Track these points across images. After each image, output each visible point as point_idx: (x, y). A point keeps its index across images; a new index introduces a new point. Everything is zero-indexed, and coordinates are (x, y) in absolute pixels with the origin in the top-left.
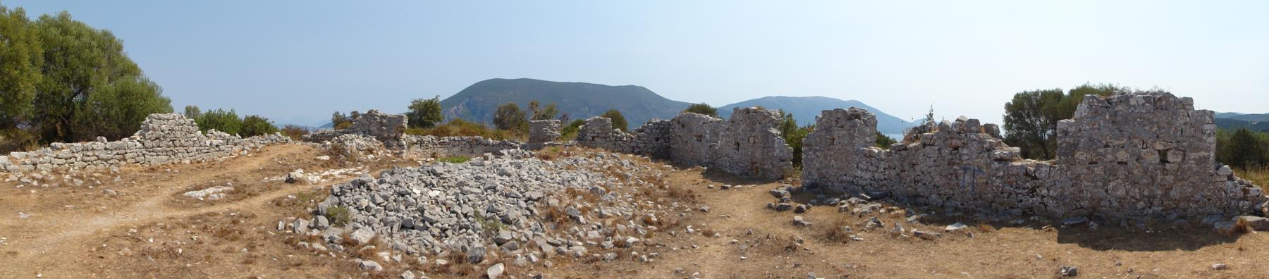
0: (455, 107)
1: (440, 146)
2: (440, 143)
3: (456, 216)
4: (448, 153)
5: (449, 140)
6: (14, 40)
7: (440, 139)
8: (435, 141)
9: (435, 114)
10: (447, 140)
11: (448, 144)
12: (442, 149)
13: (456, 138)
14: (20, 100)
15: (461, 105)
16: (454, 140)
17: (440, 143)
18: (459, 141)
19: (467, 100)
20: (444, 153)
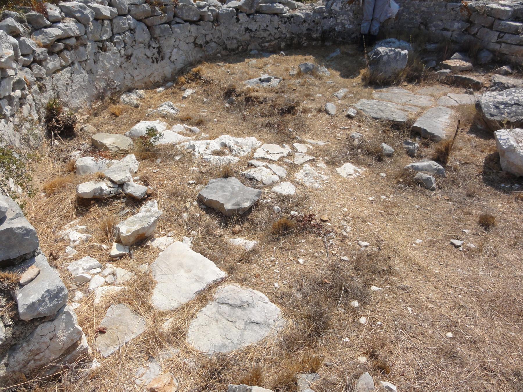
12: (65, 74)
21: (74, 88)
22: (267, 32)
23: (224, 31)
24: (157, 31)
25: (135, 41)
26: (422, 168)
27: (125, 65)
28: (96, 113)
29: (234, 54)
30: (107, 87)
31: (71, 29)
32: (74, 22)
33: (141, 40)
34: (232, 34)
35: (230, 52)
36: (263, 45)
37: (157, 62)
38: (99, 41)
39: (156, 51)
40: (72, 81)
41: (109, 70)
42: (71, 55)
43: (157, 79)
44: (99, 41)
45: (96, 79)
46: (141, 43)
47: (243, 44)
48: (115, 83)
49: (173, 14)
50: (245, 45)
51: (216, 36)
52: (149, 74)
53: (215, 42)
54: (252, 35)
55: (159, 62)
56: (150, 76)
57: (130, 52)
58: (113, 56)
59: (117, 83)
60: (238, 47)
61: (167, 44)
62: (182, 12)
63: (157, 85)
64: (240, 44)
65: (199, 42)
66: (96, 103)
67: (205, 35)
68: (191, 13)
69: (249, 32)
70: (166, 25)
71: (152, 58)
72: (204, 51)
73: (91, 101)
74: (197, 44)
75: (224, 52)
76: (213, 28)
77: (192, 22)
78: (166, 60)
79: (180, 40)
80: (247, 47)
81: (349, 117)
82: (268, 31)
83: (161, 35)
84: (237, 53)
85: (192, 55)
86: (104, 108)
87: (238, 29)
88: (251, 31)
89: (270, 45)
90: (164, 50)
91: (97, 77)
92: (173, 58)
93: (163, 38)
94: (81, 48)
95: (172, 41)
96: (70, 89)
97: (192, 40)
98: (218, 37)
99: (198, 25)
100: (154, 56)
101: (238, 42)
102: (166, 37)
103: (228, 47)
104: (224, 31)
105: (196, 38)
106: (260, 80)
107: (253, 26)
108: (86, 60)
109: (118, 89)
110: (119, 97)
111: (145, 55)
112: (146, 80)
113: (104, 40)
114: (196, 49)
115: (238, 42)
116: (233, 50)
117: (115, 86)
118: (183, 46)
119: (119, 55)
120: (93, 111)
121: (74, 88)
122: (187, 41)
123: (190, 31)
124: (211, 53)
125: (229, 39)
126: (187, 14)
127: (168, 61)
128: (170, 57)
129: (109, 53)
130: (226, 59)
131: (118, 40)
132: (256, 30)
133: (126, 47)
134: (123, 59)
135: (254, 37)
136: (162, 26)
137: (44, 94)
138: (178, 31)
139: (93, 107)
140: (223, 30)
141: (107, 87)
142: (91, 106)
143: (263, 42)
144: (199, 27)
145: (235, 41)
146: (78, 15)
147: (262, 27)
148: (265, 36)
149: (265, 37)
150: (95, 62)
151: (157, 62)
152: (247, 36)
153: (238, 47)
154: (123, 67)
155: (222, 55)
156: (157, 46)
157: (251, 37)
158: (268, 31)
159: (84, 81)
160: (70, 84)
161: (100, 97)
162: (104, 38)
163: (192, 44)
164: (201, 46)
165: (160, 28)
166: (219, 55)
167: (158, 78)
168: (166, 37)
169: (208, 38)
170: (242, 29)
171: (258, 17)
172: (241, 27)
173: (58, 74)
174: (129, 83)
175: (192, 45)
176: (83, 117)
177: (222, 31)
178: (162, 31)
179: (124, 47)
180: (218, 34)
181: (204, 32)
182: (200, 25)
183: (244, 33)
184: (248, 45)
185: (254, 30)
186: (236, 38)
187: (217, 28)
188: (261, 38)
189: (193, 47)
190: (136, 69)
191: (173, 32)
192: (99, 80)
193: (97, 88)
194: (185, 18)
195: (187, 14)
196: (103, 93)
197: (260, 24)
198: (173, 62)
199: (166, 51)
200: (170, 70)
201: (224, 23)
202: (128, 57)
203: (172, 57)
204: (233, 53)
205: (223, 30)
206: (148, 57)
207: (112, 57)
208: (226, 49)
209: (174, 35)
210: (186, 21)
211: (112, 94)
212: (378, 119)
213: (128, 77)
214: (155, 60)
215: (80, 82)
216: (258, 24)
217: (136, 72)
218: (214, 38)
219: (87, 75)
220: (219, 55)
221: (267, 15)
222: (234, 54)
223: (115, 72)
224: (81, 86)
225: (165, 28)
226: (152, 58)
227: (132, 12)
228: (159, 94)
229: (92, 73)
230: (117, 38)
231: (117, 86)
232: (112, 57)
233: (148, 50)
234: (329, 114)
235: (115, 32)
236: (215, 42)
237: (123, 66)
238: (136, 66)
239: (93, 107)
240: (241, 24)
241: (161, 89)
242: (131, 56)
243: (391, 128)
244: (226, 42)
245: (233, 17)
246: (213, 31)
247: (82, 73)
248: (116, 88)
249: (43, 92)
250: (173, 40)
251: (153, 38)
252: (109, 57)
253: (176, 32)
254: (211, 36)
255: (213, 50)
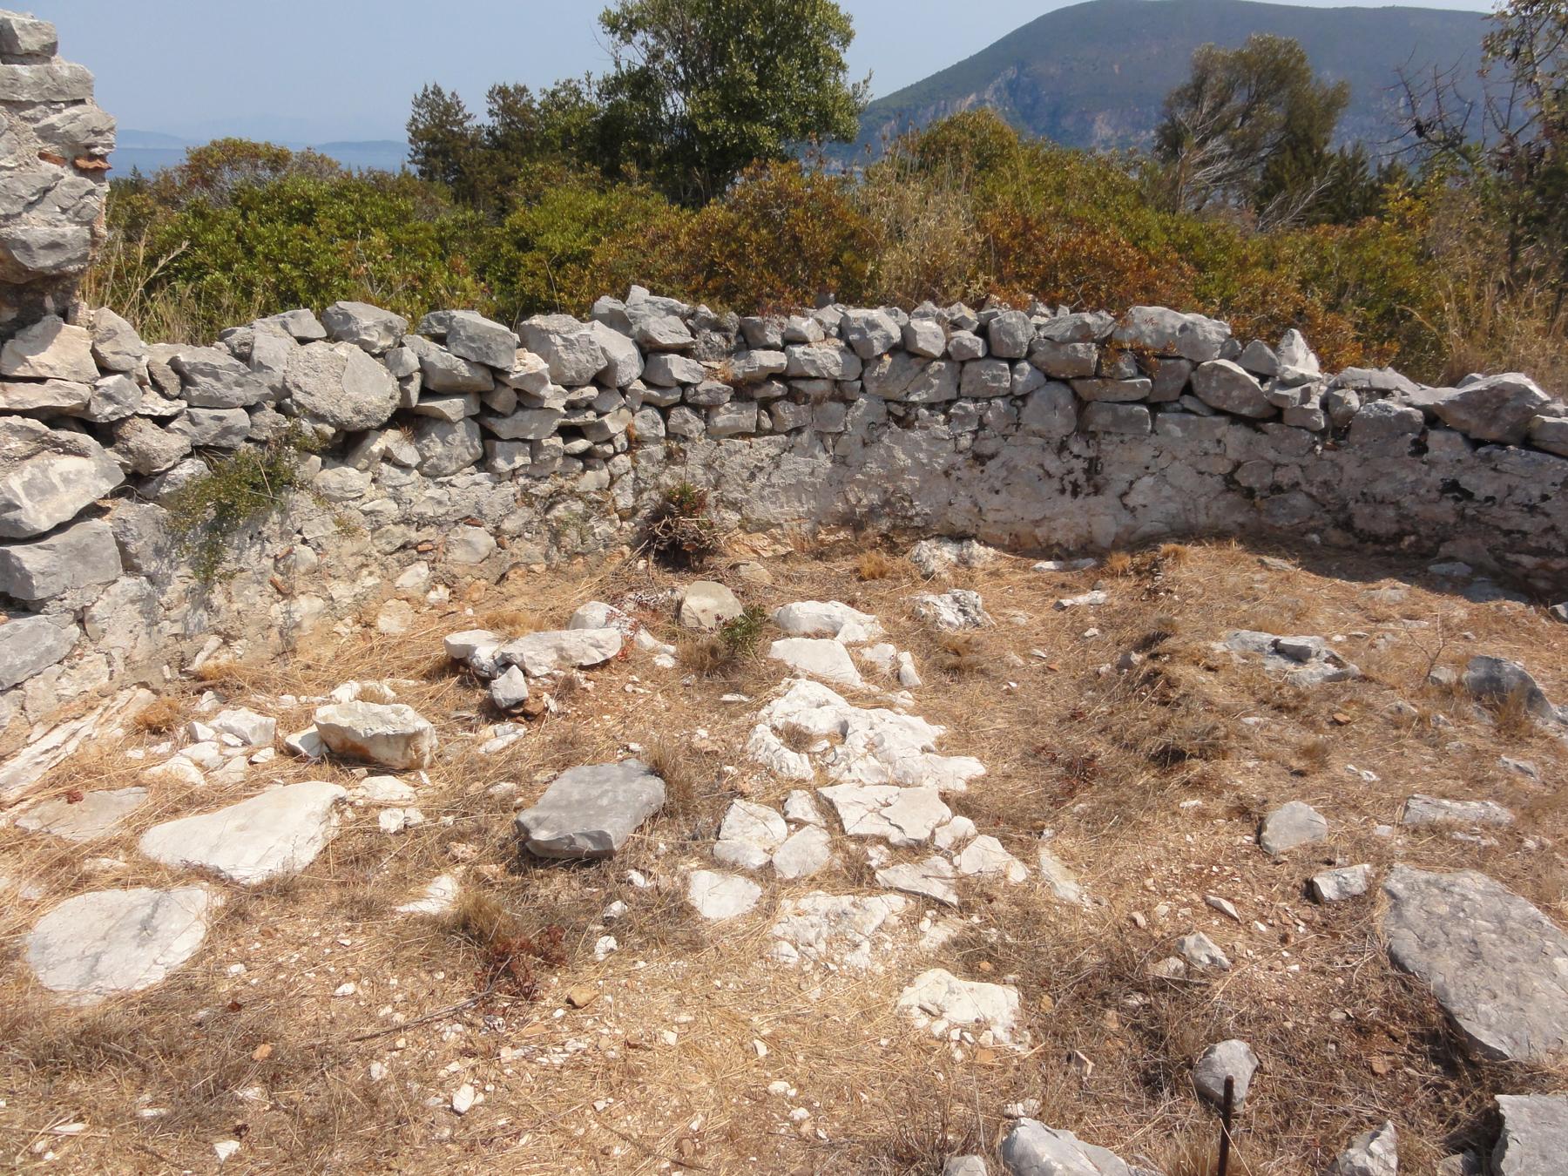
0: (973, 97)
1: (747, 417)
2: (743, 390)
3: (373, 345)
4: (836, 483)
5: (851, 341)
6: (1032, 222)
7: (747, 341)
8: (680, 368)
9: (788, 68)
10: (826, 356)
11: (840, 393)
12: (765, 448)
13: (929, 333)
14: (1275, 338)
15: (991, 87)
16: (904, 348)
17: (743, 390)
18: (956, 359)
19: (1011, 73)
20: (797, 489)
21: (774, 480)
22: (1540, 518)
23: (1352, 470)
24: (1101, 419)
25: (1018, 425)
26: (1023, 1157)
27: (965, 474)
28: (822, 553)
29: (1376, 554)
30: (883, 507)
31: (814, 362)
32: (838, 348)
33: (1035, 426)
34: (1382, 488)
35: (1361, 541)
36: (1511, 557)
37: (1075, 494)
38: (899, 403)
39: (1080, 465)
40: (778, 466)
41: (903, 470)
42: (797, 414)
43: (1058, 537)
44: (899, 403)
45: (853, 481)
46: (1034, 434)
47: (1423, 530)
48: (912, 506)
49: (1181, 383)
50: (1429, 537)
51: (1319, 479)
52: (1038, 517)
53: (1310, 495)
54: (1470, 512)
55: (1081, 496)
56: (1037, 523)
57: (988, 447)
58: (930, 444)
59: (920, 506)
60: (1400, 536)
61: (1120, 459)
62: (1208, 386)
63: (1047, 551)
64: (1408, 528)
65: (1246, 478)
66: (830, 532)
67: (1276, 466)
68: (1235, 393)
69: (1457, 500)
70: (1137, 408)
71: (1062, 479)
72: (1259, 512)
73: (820, 523)
74: (1237, 483)
75: (1336, 536)
76: (1312, 450)
77: (1236, 419)
78: (1108, 499)
79: (1175, 458)
80: (1438, 544)
81: (1311, 893)
82: (1547, 515)
83: (1112, 429)
84: (1389, 554)
85: (1207, 507)
86: (851, 550)
87: (1412, 478)
88: (1469, 496)
89: (1544, 566)
90: (1107, 470)
91: (859, 476)
92: (1134, 499)
93: (1116, 439)
94: (836, 407)
95: (1145, 454)
96: (761, 479)
97: (1224, 467)
98: (1325, 483)
99: (1258, 430)
100: (1072, 478)
101: (1402, 517)
102: (1126, 438)
103: (1359, 523)
104: (1352, 470)
105: (1238, 465)
106: (1275, 643)
107: (1481, 483)
108: (840, 434)
109: (918, 522)
110: (915, 542)
111: (1041, 466)
112: (1018, 528)
113: (914, 404)
114: (1230, 496)
115: (1402, 517)
116: (1376, 539)
117: (912, 512)
118: (1182, 475)
119: (950, 446)
120: (813, 544)
121: (774, 480)
122: (1202, 467)
123: (1219, 441)
124: (1283, 522)
125: (1365, 497)
126: (1221, 393)
127: (1117, 502)
128: (1125, 494)
129: (917, 435)
130: (1319, 561)
131: (961, 412)
132: (1488, 499)
133: (981, 434)
134: (960, 458)
135: (1474, 520)
136: (1123, 410)
137: (677, 469)
138: (1177, 432)
139: (820, 537)
140: (1350, 466)
141: (883, 507)
142: (815, 534)
143: (1511, 548)
144: (1258, 436)
145: (1391, 512)
146: (854, 337)
147: (1519, 496)
148: (1526, 527)
149: (1524, 534)
150: (865, 444)
151: (1075, 494)
152: (1446, 510)
153: (1400, 536)
154: (953, 477)
155: (1325, 543)
156: (1091, 453)
157: (1461, 515)
158: (1547, 515)
159: (812, 473)
160: (769, 470)
161: (851, 521)
162: (914, 398)
163: (1220, 478)
164: (1250, 493)
165: (1115, 411)
166: (1315, 537)
167: (1062, 533)
168: (1126, 438)
169: (1284, 477)
170: (1429, 480)
171: (1514, 456)
172: (1428, 474)
173: (738, 442)
174: (960, 521)
175: (1216, 483)
176: (778, 547)
177: (1347, 468)
178: (1118, 421)
179: (975, 432)
180: (1328, 474)
181: (1271, 455)
182: (1264, 433)
183: (1434, 495)
184: (1443, 540)
185: (1480, 494)
186: (1397, 504)
187: (1328, 454)
188: (1508, 533)
189: (1220, 487)
190: (997, 492)
191: (1153, 431)
192: (864, 486)
193: (847, 501)
194: (1214, 404)
195: (1221, 393)
196: (862, 515)
197: (1514, 481)
198: (1133, 510)
199: (1118, 478)
200: (1113, 529)
201: (1361, 446)
202: (980, 459)
203: (1132, 494)
204: (1370, 547)
205: (1350, 466)
206: (1049, 475)
207: (925, 445)
208: (1347, 525)
209: (1154, 439)
210: (1218, 412)
211: (894, 527)
212: (1403, 968)
213: (963, 502)
214: (1069, 488)
215: (800, 474)
216: (1506, 479)
217: (996, 501)
218: (1310, 483)
219: (829, 465)
220: (1315, 537)
221: (1552, 459)
222: (1376, 554)
223: (924, 481)
224: (800, 482)
225: (1131, 415)
226: (1062, 479)
227: (1035, 357)
228: (1031, 575)
229: (844, 463)
230: (960, 407)
231: (917, 514)
232: (925, 445)
233: (1054, 457)
234: (1258, 841)
235: (963, 391)
236: (1310, 495)
237: (955, 474)
238: (998, 485)
239: (820, 537)
240: (1432, 464)
241: (1049, 565)
242: (992, 457)
243: (1421, 1038)
244: (1352, 504)
245: (1403, 434)
246: (1308, 460)
247: (813, 456)
248: (911, 519)
249: (675, 464)
250: (1150, 452)
251: (1084, 431)
252: (917, 443)
253: (1168, 433)
254: (1298, 472)
255: (1293, 516)
